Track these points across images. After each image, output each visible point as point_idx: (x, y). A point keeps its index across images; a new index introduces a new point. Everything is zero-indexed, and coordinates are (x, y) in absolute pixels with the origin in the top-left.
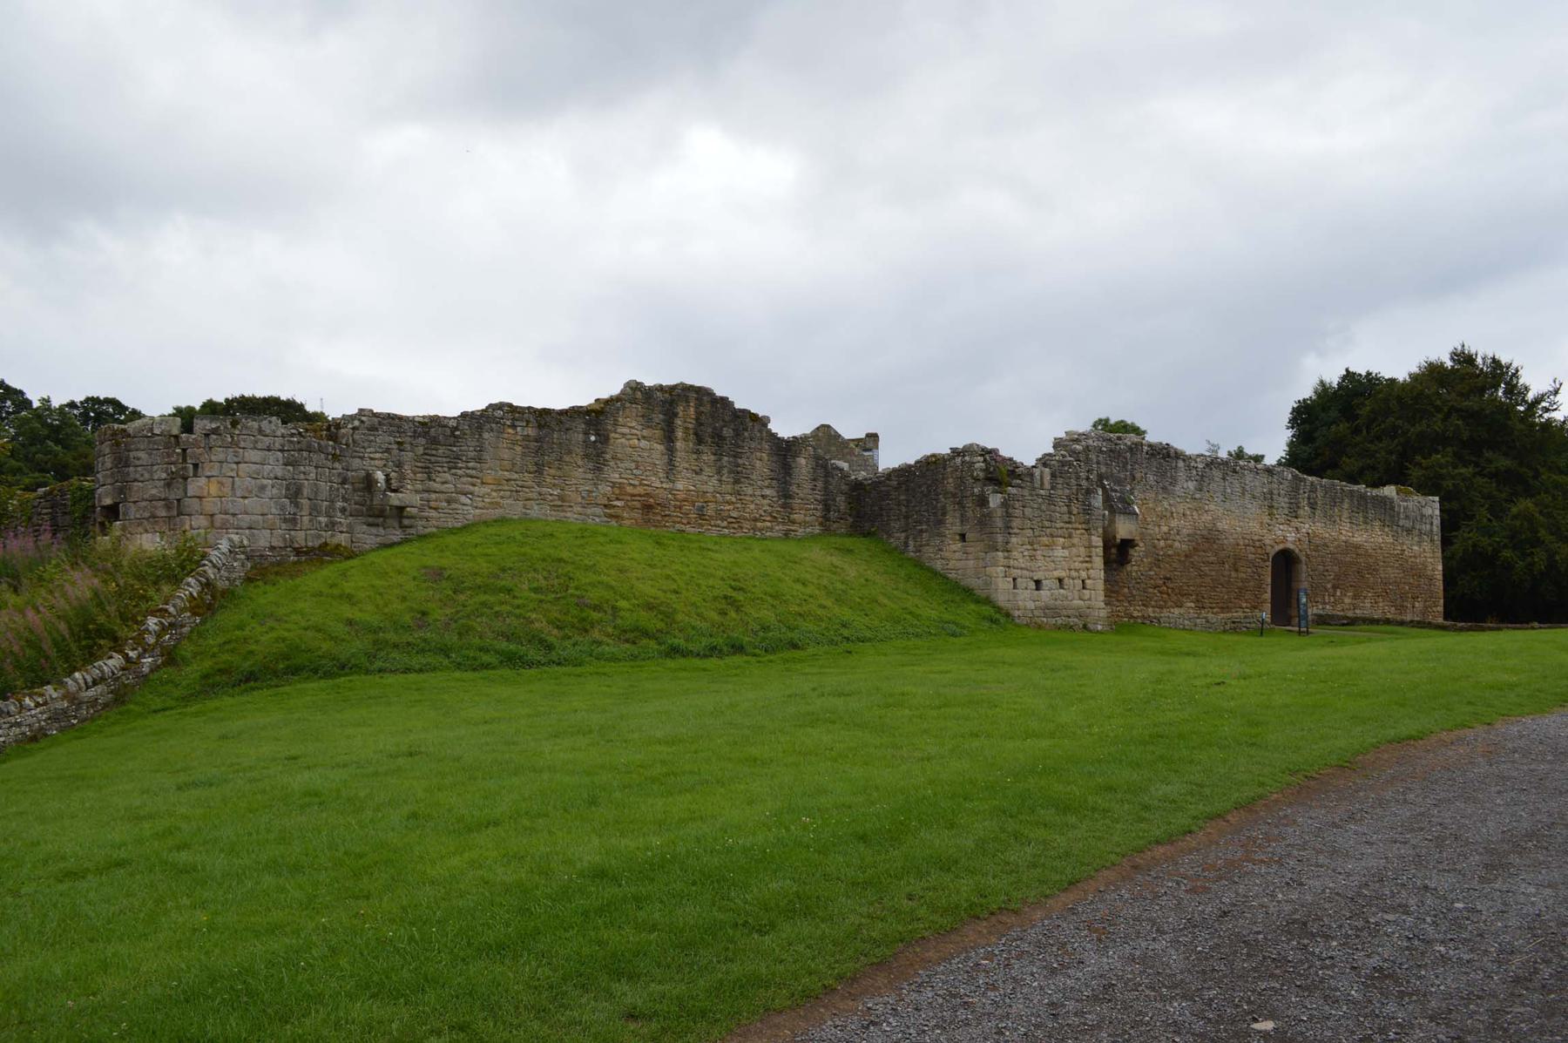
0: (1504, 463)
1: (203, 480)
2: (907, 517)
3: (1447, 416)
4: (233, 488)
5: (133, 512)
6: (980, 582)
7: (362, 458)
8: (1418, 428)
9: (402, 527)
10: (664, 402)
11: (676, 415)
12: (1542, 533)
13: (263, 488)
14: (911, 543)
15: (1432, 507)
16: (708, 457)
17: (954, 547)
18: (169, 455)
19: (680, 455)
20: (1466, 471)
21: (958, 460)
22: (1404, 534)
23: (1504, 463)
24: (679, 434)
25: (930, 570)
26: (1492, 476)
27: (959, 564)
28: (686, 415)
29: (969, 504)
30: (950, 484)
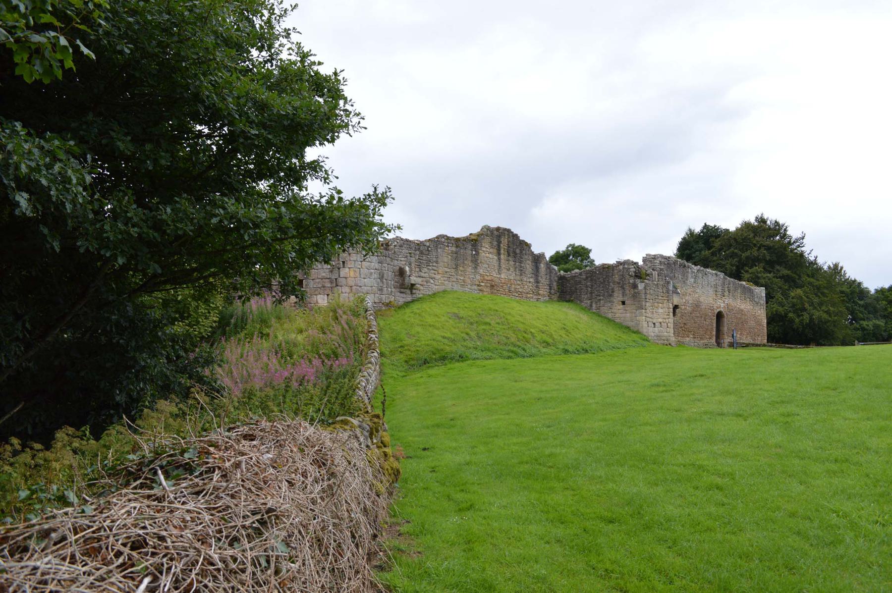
0: (786, 272)
1: (347, 269)
2: (591, 293)
3: (760, 248)
8: (748, 253)
12: (807, 305)
14: (594, 305)
15: (761, 292)
16: (512, 263)
19: (502, 261)
20: (770, 275)
21: (621, 267)
22: (750, 305)
23: (786, 272)
24: (502, 251)
25: (606, 318)
26: (780, 277)
28: (504, 241)
29: (627, 287)
30: (617, 278)
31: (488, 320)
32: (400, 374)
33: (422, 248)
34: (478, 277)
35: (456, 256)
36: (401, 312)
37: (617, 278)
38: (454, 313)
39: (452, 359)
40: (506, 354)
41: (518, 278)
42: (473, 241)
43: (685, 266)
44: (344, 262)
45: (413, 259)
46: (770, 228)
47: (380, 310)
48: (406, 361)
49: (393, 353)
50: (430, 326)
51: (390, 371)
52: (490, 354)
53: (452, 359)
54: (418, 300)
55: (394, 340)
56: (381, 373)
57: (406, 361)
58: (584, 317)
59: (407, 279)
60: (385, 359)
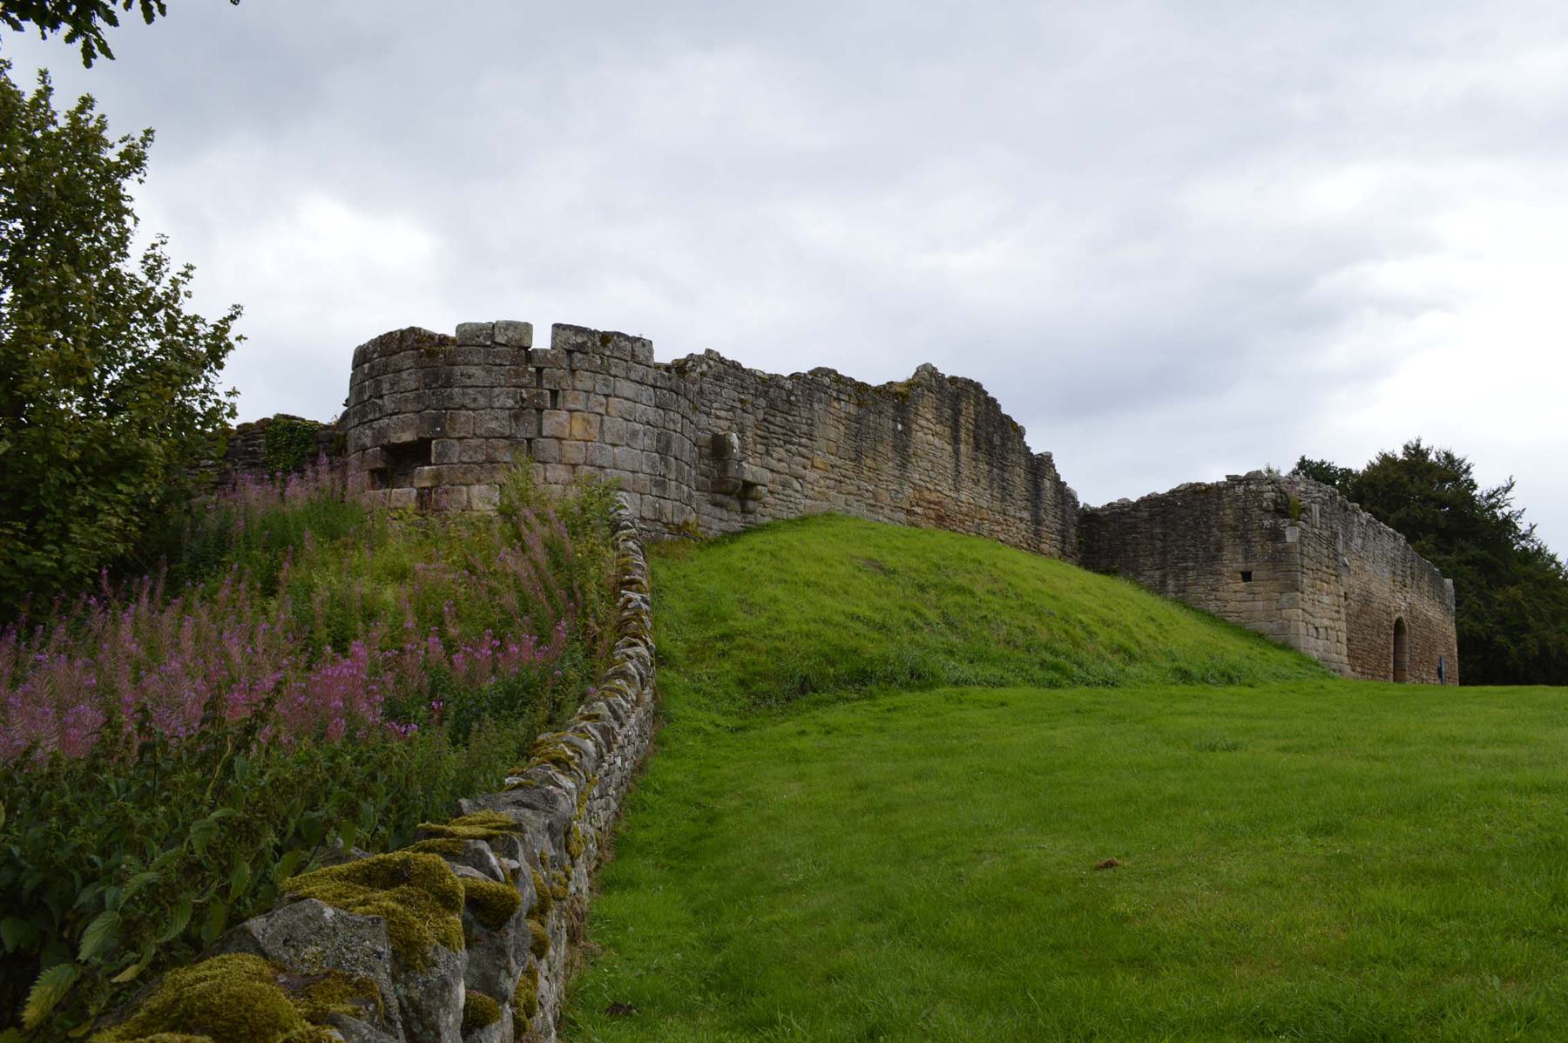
0: (1475, 552)
2: (1164, 553)
4: (602, 432)
5: (456, 452)
6: (1273, 626)
7: (708, 414)
9: (745, 511)
11: (960, 411)
14: (1171, 583)
16: (984, 467)
17: (1235, 587)
19: (963, 459)
21: (1240, 490)
23: (1475, 552)
24: (963, 435)
27: (1243, 606)
28: (968, 410)
29: (1256, 538)
30: (1229, 515)
31: (960, 580)
32: (721, 721)
35: (858, 431)
36: (717, 553)
37: (1229, 515)
38: (870, 560)
39: (891, 679)
40: (1038, 673)
41: (997, 505)
42: (894, 400)
43: (1346, 509)
44: (554, 394)
45: (750, 419)
46: (1432, 464)
47: (656, 541)
48: (741, 682)
49: (696, 654)
50: (808, 584)
51: (689, 711)
52: (997, 671)
53: (891, 679)
54: (761, 528)
55: (701, 617)
56: (659, 715)
57: (741, 682)
58: (1157, 606)
59: (732, 471)
60: (671, 674)
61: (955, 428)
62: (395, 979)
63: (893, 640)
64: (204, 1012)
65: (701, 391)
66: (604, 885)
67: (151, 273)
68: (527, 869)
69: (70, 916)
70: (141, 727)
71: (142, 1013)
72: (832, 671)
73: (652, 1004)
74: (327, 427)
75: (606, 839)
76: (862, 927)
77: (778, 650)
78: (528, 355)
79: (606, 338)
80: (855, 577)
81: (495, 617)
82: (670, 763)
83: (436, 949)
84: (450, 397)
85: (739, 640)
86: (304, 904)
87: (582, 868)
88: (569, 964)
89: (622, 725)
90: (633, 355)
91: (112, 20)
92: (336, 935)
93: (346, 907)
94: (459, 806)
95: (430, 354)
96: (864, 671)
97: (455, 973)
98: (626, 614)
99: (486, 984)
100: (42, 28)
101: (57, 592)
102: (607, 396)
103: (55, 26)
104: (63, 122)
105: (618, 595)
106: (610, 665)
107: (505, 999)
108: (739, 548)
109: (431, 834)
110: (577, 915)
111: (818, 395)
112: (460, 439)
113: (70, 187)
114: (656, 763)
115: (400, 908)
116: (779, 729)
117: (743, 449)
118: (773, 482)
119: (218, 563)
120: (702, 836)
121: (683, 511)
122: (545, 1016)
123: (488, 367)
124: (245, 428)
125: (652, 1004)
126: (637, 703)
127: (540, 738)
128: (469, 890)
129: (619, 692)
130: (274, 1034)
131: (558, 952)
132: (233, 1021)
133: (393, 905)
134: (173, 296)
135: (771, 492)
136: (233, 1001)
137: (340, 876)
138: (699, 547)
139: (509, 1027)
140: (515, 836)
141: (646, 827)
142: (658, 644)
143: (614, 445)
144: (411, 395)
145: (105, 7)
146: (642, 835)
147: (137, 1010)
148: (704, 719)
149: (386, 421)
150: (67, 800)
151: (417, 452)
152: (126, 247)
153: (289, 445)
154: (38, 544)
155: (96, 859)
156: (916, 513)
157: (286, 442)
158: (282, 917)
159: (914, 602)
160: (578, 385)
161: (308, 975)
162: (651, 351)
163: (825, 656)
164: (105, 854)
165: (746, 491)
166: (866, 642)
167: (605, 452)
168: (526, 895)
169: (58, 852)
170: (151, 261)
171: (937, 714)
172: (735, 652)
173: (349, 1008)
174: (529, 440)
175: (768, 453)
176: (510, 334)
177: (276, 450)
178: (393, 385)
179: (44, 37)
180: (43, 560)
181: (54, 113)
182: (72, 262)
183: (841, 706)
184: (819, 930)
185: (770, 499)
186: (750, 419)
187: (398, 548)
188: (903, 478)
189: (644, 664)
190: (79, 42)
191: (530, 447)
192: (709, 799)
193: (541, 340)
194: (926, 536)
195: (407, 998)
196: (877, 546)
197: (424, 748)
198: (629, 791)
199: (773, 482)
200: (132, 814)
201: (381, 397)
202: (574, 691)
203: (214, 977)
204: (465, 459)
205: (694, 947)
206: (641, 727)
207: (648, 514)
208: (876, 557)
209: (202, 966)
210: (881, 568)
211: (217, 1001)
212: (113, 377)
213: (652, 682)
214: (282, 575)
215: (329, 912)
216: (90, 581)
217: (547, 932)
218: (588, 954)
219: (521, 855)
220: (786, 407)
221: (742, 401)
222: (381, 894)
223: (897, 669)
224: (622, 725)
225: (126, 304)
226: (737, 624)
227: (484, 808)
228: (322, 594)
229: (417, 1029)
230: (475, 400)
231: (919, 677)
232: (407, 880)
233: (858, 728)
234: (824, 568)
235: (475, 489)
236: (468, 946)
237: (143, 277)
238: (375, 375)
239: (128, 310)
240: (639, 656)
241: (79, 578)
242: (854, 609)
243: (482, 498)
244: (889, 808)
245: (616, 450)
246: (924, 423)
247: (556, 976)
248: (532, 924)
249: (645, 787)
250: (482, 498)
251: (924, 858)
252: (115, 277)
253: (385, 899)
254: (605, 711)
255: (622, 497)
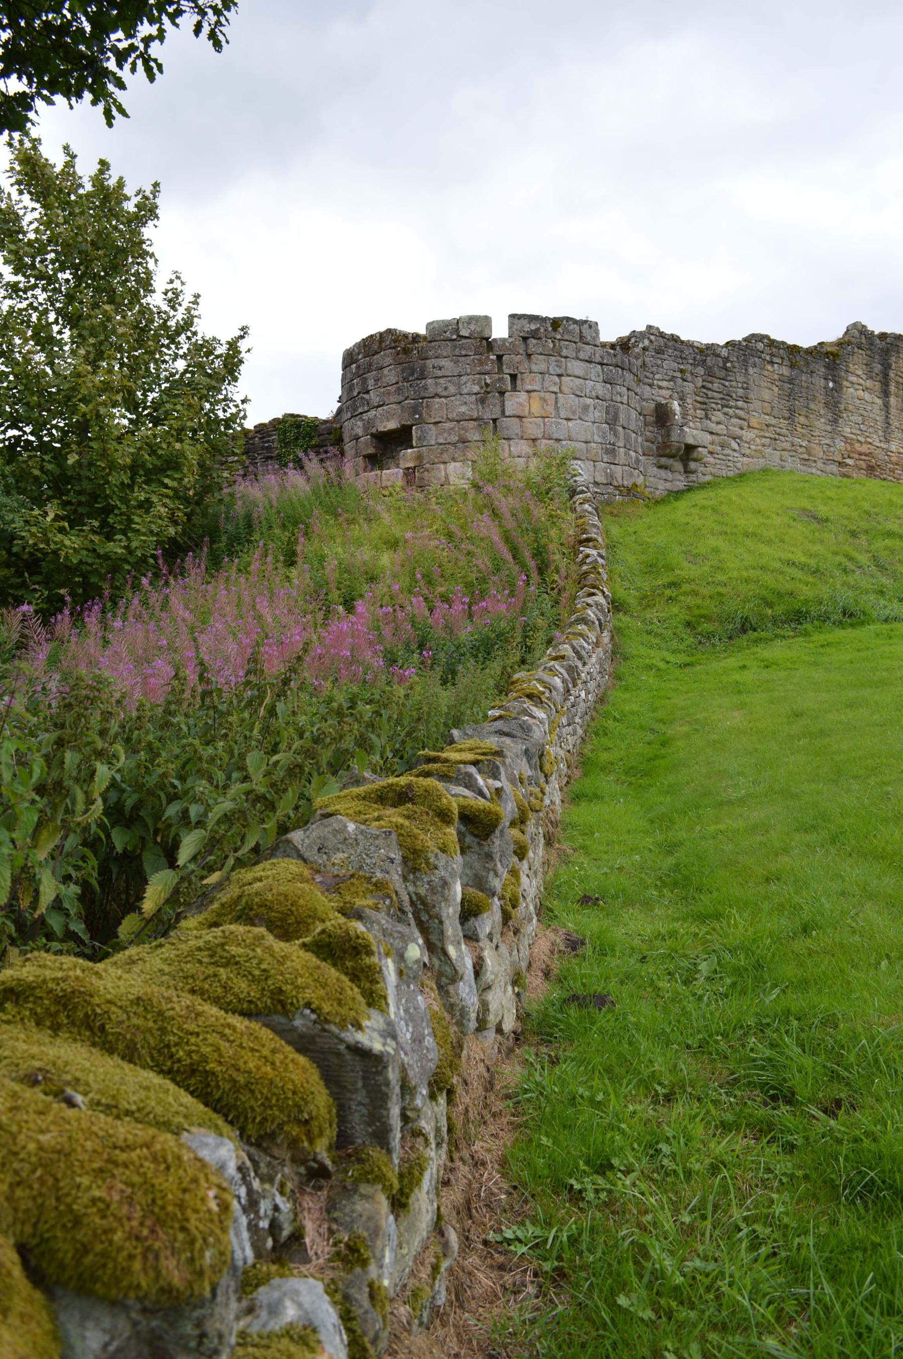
1: (523, 396)
4: (557, 408)
5: (433, 435)
7: (651, 385)
9: (687, 471)
10: (882, 350)
13: (586, 408)
18: (481, 363)
19: (893, 411)
32: (671, 658)
33: (710, 361)
34: (840, 445)
35: (791, 390)
36: (662, 510)
38: (804, 510)
39: (824, 618)
42: (828, 358)
44: (514, 377)
45: (689, 387)
47: (608, 503)
48: (688, 624)
49: (647, 602)
50: (746, 535)
51: (643, 650)
53: (824, 618)
54: (703, 486)
55: (651, 568)
56: (616, 654)
57: (688, 624)
59: (675, 436)
60: (626, 619)
61: (885, 383)
62: (405, 879)
63: (826, 583)
64: (261, 906)
65: (644, 365)
66: (575, 798)
67: (173, 303)
68: (508, 787)
69: (160, 825)
70: (201, 677)
71: (216, 905)
72: (770, 612)
73: (615, 897)
74: (326, 422)
75: (574, 759)
76: (797, 837)
77: (720, 594)
78: (488, 344)
79: (556, 323)
80: (790, 527)
81: (473, 577)
82: (627, 695)
83: (436, 856)
84: (425, 388)
85: (686, 587)
86: (332, 820)
87: (555, 783)
88: (546, 863)
89: (584, 664)
90: (581, 337)
91: (121, 85)
92: (358, 844)
93: (364, 822)
94: (451, 736)
95: (406, 351)
96: (799, 612)
97: (453, 875)
98: (585, 568)
99: (479, 882)
100: (69, 99)
101: (129, 572)
102: (560, 376)
103: (79, 96)
104: (88, 187)
105: (576, 553)
106: (574, 612)
107: (494, 894)
108: (682, 505)
109: (430, 760)
110: (551, 822)
111: (752, 360)
112: (436, 423)
113: (102, 240)
114: (616, 695)
115: (407, 823)
116: (722, 664)
117: (684, 415)
118: (712, 443)
119: (249, 541)
120: (656, 757)
121: (631, 475)
122: (527, 906)
123: (456, 358)
124: (261, 429)
125: (615, 897)
126: (597, 644)
127: (516, 676)
128: (462, 808)
129: (581, 635)
130: (314, 923)
131: (537, 853)
132: (282, 913)
133: (401, 820)
134: (187, 325)
135: (711, 453)
136: (282, 898)
137: (358, 797)
138: (647, 506)
139: (498, 916)
140: (498, 761)
141: (607, 749)
142: (613, 593)
143: (568, 419)
144: (392, 389)
145: (114, 74)
146: (604, 757)
147: (211, 902)
148: (656, 657)
149: (373, 412)
150: (151, 737)
151: (400, 438)
152: (151, 285)
153: (297, 439)
154: (109, 538)
155: (176, 782)
156: (847, 465)
157: (294, 436)
158: (316, 830)
159: (846, 547)
160: (534, 368)
161: (337, 876)
162: (597, 332)
163: (763, 599)
164: (183, 779)
165: (688, 453)
166: (802, 586)
167: (563, 426)
168: (508, 810)
169: (147, 778)
170: (170, 295)
171: (868, 649)
172: (682, 598)
173: (370, 902)
174: (494, 420)
175: (707, 417)
176: (472, 327)
177: (287, 444)
178: (377, 380)
179: (71, 108)
180: (116, 548)
181: (80, 178)
182: (111, 301)
183: (778, 642)
184: (759, 838)
185: (710, 459)
186: (689, 387)
187: (388, 522)
188: (835, 433)
189: (602, 611)
190: (101, 106)
191: (495, 427)
192: (662, 726)
193: (500, 331)
194: (857, 486)
195: (416, 894)
196: (811, 497)
197: (418, 687)
198: (593, 719)
199: (712, 443)
200: (200, 749)
201: (368, 392)
202: (541, 636)
203: (267, 877)
204: (441, 441)
205: (650, 851)
206: (601, 665)
207: (601, 479)
208: (809, 507)
209: (258, 868)
210: (815, 518)
211: (270, 898)
212: (151, 396)
213: (610, 626)
214: (299, 549)
215: (351, 827)
216: (151, 561)
217: (526, 838)
218: (561, 853)
219: (503, 776)
220: (723, 374)
221: (681, 371)
222: (392, 811)
223: (830, 609)
224: (584, 664)
225: (151, 335)
226: (682, 573)
227: (471, 737)
228: (331, 564)
229: (424, 918)
230: (446, 388)
231: (851, 615)
232: (411, 800)
233: (794, 663)
234: (761, 520)
235: (452, 466)
236: (463, 852)
237: (165, 307)
238: (361, 375)
239: (157, 337)
240: (597, 604)
241: (143, 560)
242: (790, 556)
243: (457, 474)
244: (823, 733)
245: (570, 424)
246: (854, 379)
247: (535, 873)
248: (515, 832)
249: (607, 715)
250: (457, 474)
251: (855, 777)
252: (145, 310)
253: (394, 816)
254: (570, 653)
255: (577, 466)
